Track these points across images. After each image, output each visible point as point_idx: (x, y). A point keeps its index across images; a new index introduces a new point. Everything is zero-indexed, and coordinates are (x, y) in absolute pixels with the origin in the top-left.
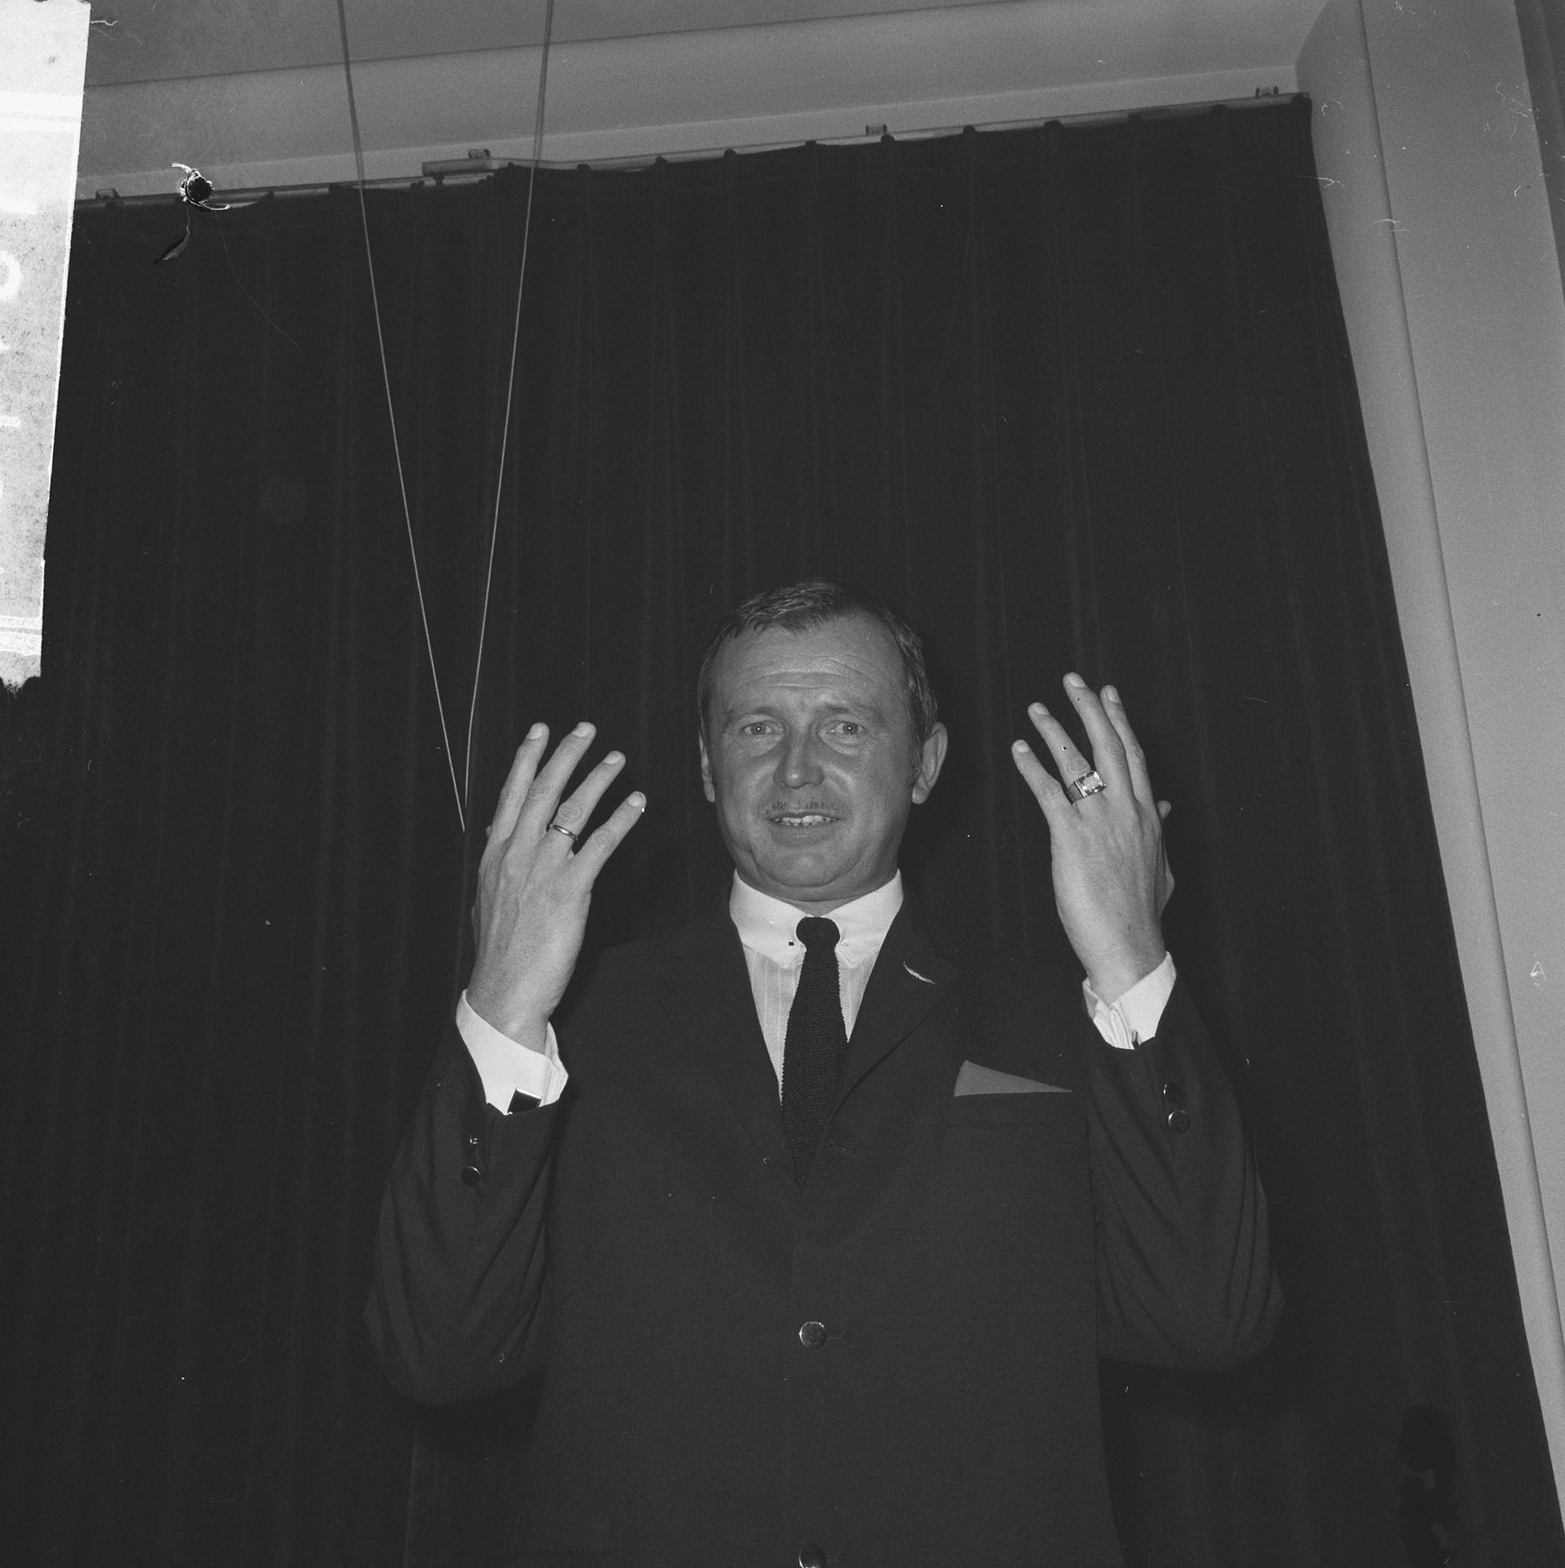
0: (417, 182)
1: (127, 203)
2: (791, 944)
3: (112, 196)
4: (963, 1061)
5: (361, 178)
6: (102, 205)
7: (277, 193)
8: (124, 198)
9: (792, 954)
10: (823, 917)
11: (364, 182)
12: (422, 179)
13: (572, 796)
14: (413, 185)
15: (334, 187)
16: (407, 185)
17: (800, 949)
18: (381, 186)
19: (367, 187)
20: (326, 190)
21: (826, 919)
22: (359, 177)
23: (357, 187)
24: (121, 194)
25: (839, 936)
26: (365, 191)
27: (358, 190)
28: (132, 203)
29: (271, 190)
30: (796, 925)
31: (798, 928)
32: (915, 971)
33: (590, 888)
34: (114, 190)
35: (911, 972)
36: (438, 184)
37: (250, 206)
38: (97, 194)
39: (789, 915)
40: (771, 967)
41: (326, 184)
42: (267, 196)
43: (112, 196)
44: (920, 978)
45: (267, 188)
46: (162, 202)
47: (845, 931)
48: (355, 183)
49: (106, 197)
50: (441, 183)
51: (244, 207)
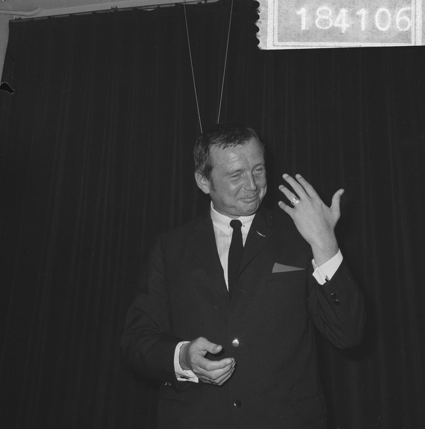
0: (199, 2)
1: (120, 10)
2: (229, 228)
3: (115, 8)
4: (275, 263)
5: (185, 1)
6: (113, 11)
7: (161, 6)
8: (119, 9)
9: (230, 231)
10: (237, 219)
11: (185, 2)
12: (201, 1)
13: (332, 204)
14: (199, 3)
15: (176, 4)
16: (197, 3)
17: (231, 230)
18: (190, 3)
19: (186, 4)
20: (174, 5)
21: (238, 220)
22: (184, 1)
23: (183, 4)
24: (118, 7)
25: (242, 224)
26: (185, 5)
27: (183, 5)
28: (121, 10)
29: (159, 5)
30: (230, 223)
31: (230, 223)
32: (260, 233)
33: (337, 246)
34: (116, 7)
35: (259, 234)
36: (205, 2)
37: (153, 10)
38: (112, 8)
39: (228, 220)
40: (224, 235)
41: (174, 3)
42: (158, 7)
43: (115, 8)
44: (261, 235)
45: (158, 5)
46: (129, 9)
47: (243, 223)
48: (183, 3)
49: (114, 9)
50: (206, 2)
51: (151, 10)
